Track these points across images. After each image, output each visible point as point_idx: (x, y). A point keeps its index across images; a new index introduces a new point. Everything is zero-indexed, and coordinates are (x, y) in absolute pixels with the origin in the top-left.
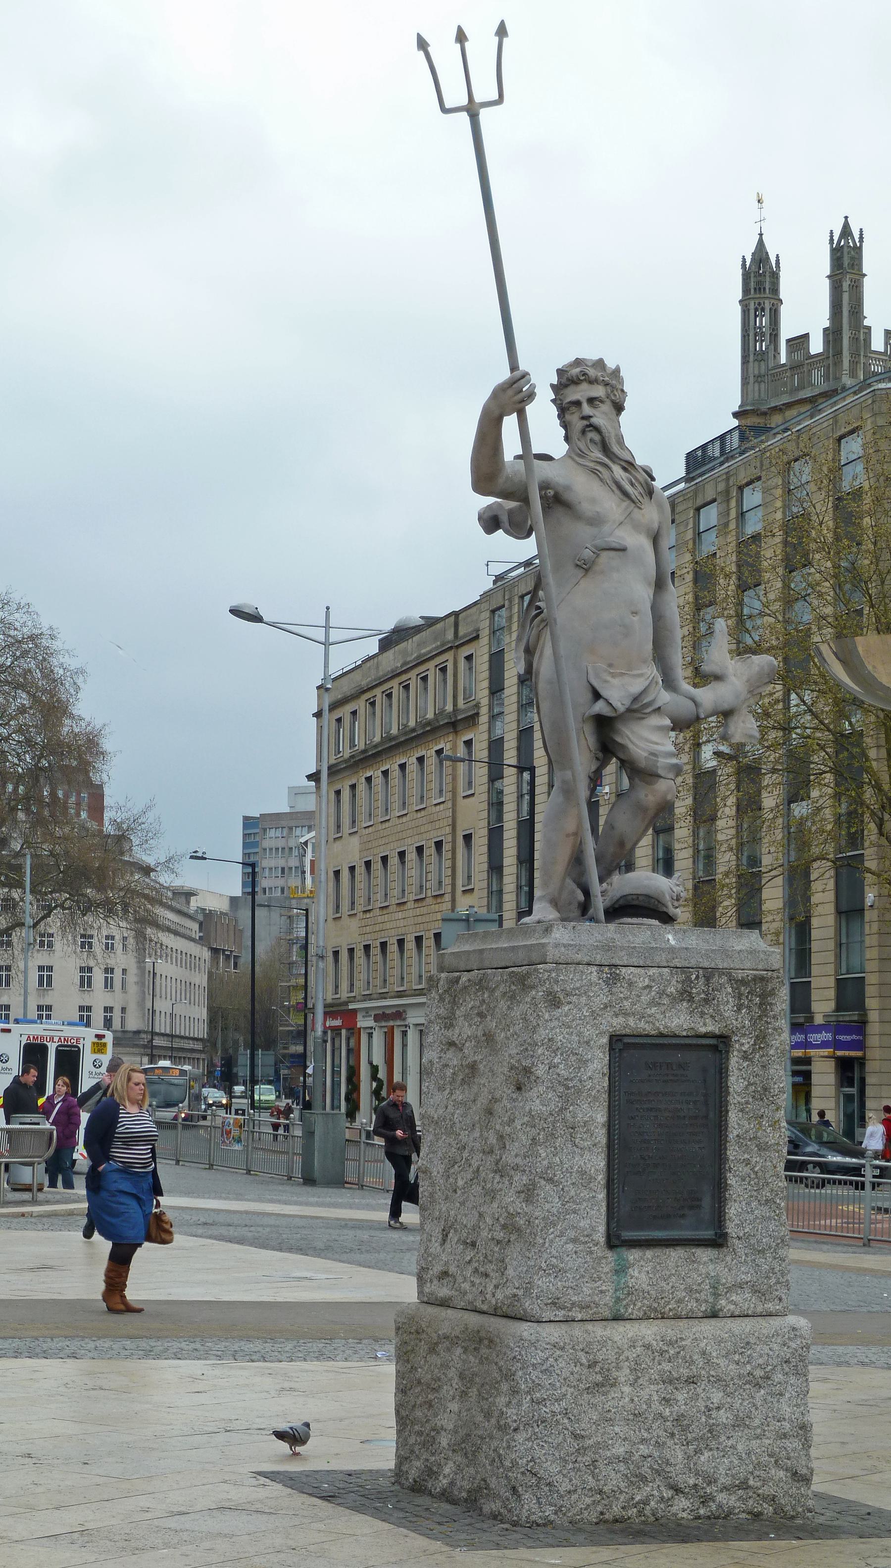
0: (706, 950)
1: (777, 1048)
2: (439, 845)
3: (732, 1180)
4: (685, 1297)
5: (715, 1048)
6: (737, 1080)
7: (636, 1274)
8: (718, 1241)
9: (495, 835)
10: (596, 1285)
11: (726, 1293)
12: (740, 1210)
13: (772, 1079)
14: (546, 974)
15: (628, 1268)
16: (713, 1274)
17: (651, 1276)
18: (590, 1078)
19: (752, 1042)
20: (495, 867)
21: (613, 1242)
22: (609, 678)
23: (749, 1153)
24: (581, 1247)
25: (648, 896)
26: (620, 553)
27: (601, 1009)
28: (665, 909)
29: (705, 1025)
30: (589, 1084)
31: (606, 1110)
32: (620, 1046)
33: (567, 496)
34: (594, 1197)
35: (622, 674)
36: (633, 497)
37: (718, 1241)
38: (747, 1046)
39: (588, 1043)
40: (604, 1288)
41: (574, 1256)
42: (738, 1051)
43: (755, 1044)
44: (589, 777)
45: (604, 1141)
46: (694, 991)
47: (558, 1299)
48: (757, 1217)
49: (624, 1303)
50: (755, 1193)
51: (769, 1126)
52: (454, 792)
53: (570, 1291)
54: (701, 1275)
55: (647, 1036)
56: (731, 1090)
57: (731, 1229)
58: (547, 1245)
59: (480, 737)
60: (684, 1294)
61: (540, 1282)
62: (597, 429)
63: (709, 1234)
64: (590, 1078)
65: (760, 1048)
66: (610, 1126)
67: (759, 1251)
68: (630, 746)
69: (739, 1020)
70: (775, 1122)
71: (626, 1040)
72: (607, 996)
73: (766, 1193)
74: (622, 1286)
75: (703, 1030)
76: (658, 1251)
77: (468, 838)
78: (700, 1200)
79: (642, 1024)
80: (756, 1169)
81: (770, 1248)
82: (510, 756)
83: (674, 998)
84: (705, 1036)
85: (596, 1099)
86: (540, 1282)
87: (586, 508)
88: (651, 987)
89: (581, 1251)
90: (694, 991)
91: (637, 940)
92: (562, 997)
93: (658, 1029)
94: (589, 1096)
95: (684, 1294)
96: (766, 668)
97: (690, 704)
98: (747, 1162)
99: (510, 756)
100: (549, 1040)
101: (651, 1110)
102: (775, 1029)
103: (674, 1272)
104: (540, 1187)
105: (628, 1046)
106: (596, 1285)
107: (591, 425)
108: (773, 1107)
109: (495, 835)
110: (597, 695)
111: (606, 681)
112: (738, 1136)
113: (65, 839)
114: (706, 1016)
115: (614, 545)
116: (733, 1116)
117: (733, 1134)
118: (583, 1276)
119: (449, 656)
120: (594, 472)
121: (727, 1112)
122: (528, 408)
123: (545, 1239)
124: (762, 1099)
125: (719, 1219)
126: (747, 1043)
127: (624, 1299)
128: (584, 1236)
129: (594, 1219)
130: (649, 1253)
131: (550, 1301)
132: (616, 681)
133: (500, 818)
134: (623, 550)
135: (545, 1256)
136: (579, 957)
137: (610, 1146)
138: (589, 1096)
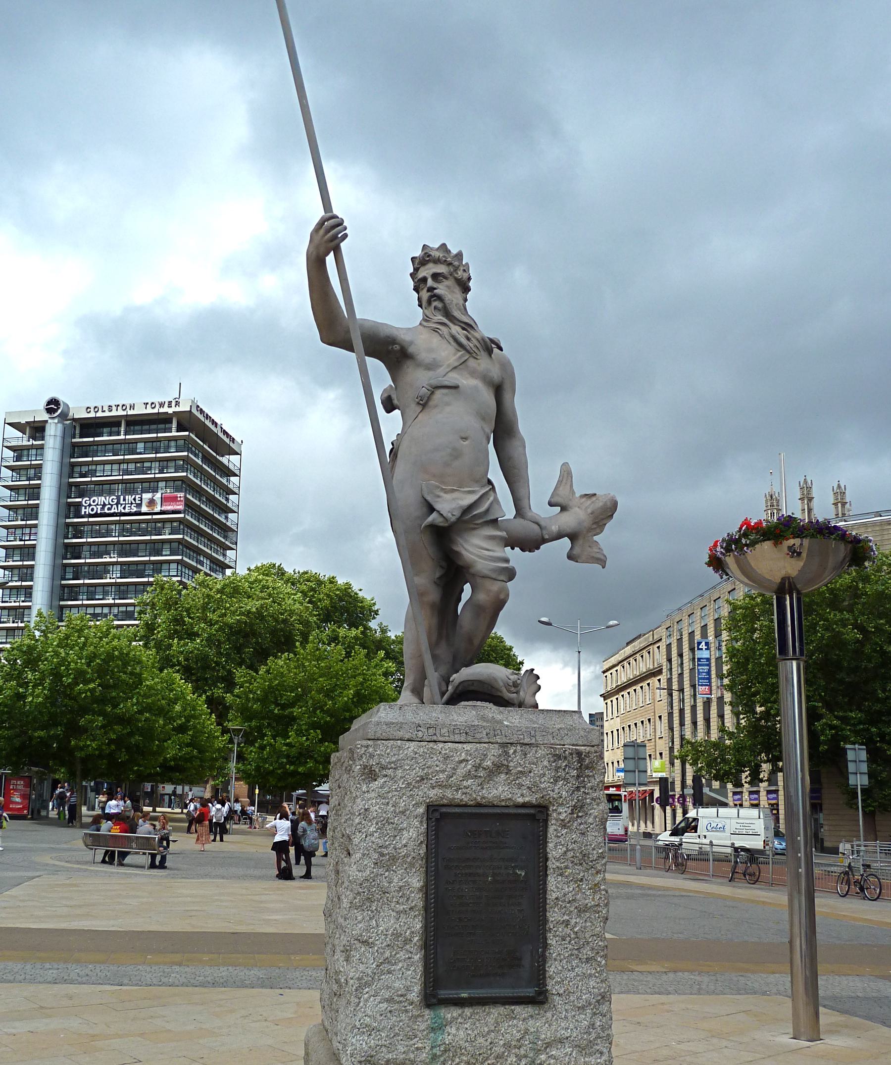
0: (527, 728)
1: (595, 817)
2: (649, 720)
3: (552, 941)
4: (504, 1053)
5: (532, 817)
6: (556, 847)
7: (453, 1031)
8: (538, 998)
9: (670, 715)
10: (412, 1042)
11: (546, 1048)
12: (560, 968)
13: (591, 845)
14: (363, 749)
15: (445, 1026)
16: (532, 1030)
17: (469, 1032)
18: (405, 846)
19: (569, 811)
20: (671, 729)
21: (432, 998)
22: (442, 494)
23: (569, 915)
24: (396, 1006)
25: (480, 682)
26: (453, 391)
27: (417, 782)
28: (500, 694)
29: (522, 795)
30: (404, 851)
31: (423, 875)
32: (437, 815)
33: (411, 350)
34: (409, 958)
35: (453, 491)
36: (468, 348)
37: (538, 998)
38: (564, 815)
39: (403, 813)
40: (420, 1045)
41: (389, 1014)
42: (557, 820)
43: (572, 813)
44: (435, 582)
45: (421, 904)
46: (511, 764)
47: (372, 1057)
48: (578, 975)
49: (442, 1059)
50: (576, 952)
51: (590, 889)
52: (654, 699)
53: (384, 1049)
54: (520, 1031)
55: (465, 806)
56: (550, 856)
57: (552, 986)
58: (361, 1004)
59: (663, 677)
60: (502, 1050)
61: (354, 1040)
62: (439, 298)
63: (530, 992)
64: (405, 846)
65: (578, 817)
66: (426, 890)
67: (579, 1008)
68: (464, 552)
69: (556, 791)
70: (595, 885)
71: (444, 810)
72: (423, 769)
73: (587, 952)
74: (439, 1043)
75: (520, 800)
76: (479, 1010)
77: (660, 717)
78: (520, 959)
79: (459, 796)
80: (576, 930)
81: (590, 1004)
82: (675, 686)
83: (491, 771)
84: (524, 805)
85: (412, 865)
86: (354, 1040)
87: (424, 356)
88: (467, 761)
89: (395, 1010)
90: (511, 764)
91: (461, 719)
92: (377, 770)
93: (475, 799)
94: (406, 862)
95: (502, 1050)
96: (609, 504)
97: (536, 527)
98: (567, 923)
99: (675, 686)
100: (366, 810)
101: (470, 874)
102: (592, 799)
103: (493, 1028)
104: (356, 949)
105: (444, 816)
106: (412, 1042)
107: (435, 295)
108: (593, 871)
109: (670, 715)
110: (431, 509)
111: (439, 497)
112: (557, 899)
113: (570, 730)
114: (523, 788)
115: (447, 383)
116: (552, 881)
117: (552, 896)
118: (398, 1035)
119: (651, 647)
120: (435, 330)
121: (547, 875)
122: (343, 245)
123: (359, 998)
124: (581, 864)
125: (539, 977)
126: (564, 812)
127: (441, 1056)
128: (398, 996)
129: (408, 976)
130: (468, 1011)
131: (363, 1059)
132: (448, 496)
133: (672, 708)
134: (456, 387)
135: (360, 1015)
136: (400, 734)
137: (426, 908)
138: (406, 862)
